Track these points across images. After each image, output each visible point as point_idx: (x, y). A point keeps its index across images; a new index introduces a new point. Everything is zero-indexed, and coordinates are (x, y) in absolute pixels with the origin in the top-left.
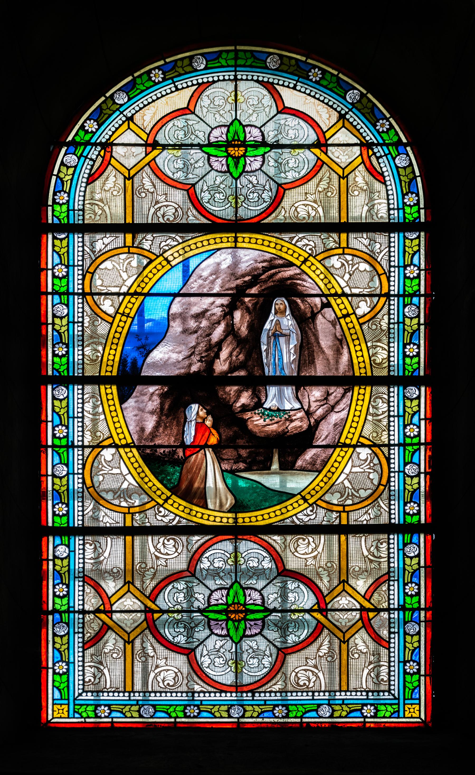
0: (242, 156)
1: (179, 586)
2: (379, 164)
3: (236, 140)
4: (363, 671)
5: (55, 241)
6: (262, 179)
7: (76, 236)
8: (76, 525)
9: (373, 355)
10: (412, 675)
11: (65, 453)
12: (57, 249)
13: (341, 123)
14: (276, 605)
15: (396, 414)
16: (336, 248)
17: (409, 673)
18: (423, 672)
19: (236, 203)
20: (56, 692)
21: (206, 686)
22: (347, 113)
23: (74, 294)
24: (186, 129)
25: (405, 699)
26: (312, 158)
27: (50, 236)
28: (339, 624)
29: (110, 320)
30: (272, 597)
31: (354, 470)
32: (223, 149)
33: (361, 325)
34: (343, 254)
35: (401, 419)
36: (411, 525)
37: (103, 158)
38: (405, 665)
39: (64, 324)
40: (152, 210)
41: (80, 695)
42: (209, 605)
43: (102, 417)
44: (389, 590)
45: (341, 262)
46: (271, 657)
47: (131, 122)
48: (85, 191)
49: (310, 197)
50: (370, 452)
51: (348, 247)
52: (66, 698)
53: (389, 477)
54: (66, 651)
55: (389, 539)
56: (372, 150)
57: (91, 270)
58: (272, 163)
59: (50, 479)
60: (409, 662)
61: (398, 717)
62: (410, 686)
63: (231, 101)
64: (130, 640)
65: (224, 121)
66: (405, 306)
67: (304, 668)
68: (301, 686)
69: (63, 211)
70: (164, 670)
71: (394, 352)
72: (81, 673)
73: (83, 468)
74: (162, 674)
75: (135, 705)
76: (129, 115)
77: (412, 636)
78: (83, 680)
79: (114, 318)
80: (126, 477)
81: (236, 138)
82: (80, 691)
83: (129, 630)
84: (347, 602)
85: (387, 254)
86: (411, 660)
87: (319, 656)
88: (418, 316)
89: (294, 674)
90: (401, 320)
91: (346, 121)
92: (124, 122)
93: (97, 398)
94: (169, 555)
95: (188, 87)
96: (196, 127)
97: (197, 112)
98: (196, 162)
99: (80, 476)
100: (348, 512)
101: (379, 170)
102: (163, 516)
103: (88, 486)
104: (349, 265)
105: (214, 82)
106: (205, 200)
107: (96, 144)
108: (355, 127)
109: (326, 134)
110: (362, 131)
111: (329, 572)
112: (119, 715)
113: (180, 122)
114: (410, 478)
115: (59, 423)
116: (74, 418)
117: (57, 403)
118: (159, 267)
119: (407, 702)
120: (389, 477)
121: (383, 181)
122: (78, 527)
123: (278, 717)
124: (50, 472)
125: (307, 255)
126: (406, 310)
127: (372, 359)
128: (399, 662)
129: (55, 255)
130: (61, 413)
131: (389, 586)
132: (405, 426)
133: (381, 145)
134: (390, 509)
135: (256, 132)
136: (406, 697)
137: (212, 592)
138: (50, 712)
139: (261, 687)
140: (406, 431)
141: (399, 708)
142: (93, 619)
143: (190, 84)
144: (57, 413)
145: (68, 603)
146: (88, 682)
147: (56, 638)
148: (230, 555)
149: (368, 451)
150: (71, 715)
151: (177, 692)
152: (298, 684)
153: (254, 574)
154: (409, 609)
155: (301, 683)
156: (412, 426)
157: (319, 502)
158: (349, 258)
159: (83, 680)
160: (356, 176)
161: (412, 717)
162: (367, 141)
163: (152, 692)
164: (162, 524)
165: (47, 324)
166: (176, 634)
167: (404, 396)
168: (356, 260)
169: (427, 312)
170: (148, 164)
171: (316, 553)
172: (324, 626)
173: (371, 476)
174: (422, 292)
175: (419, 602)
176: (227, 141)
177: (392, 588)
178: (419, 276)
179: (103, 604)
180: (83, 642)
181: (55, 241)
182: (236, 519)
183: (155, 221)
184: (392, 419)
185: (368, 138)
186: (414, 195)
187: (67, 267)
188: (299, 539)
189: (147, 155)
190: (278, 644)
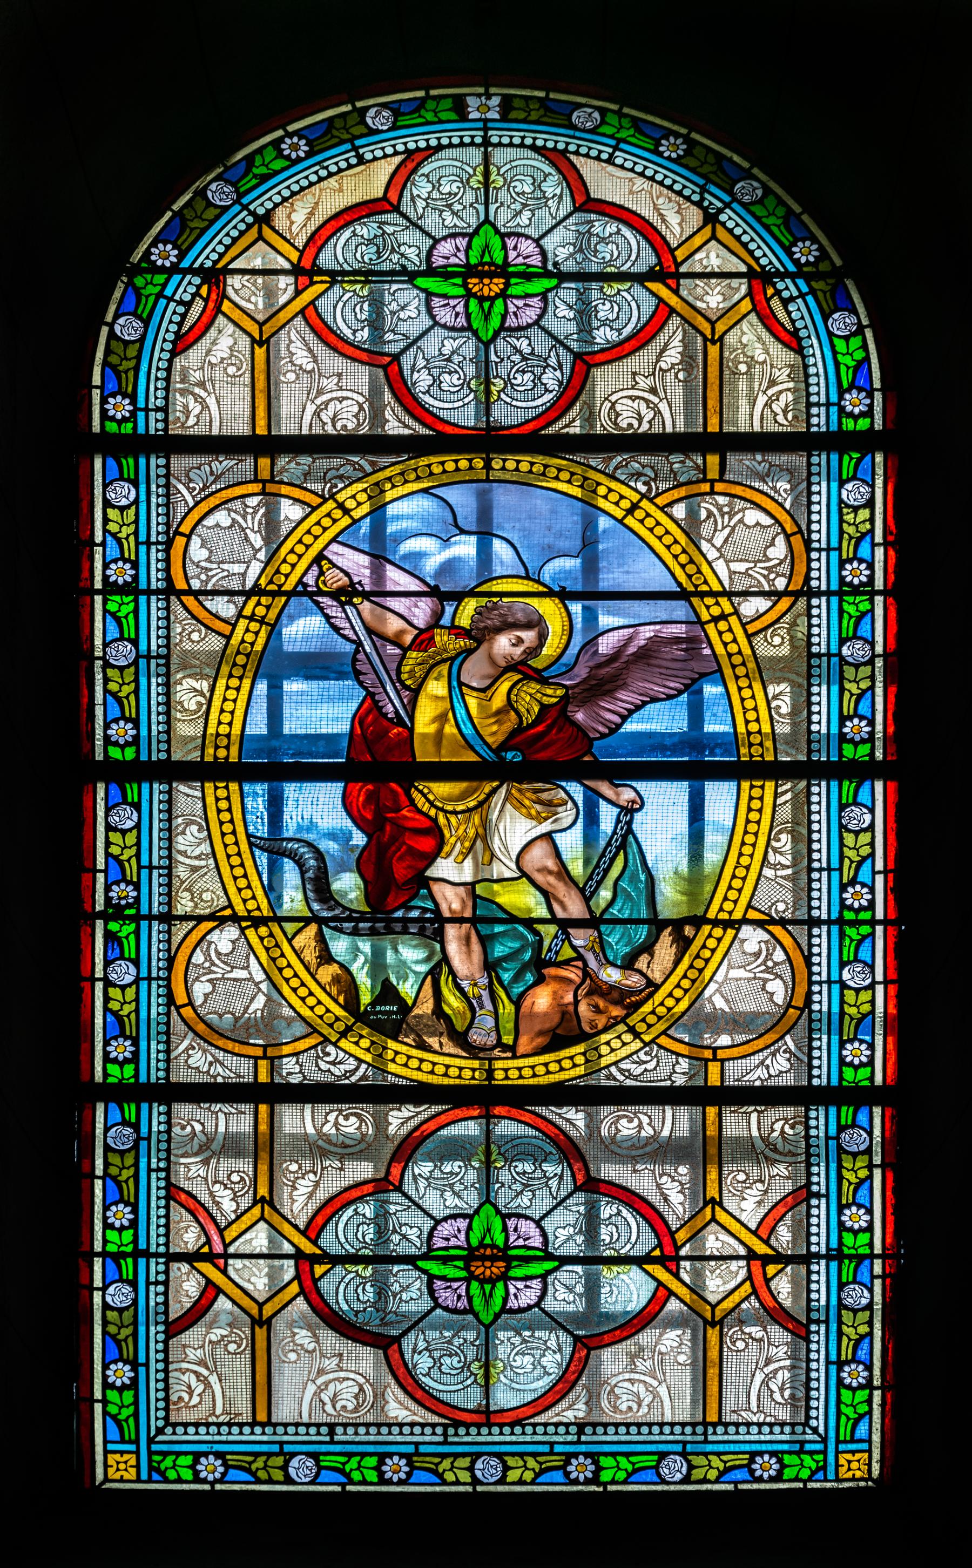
0: (497, 296)
1: (365, 231)
2: (789, 313)
3: (487, 1246)
5: (109, 511)
6: (541, 344)
9: (775, 697)
13: (708, 231)
14: (571, 1250)
16: (698, 481)
18: (877, 1383)
19: (487, 174)
21: (423, 1412)
22: (720, 211)
23: (149, 592)
24: (380, 241)
25: (838, 1442)
26: (648, 306)
28: (704, 306)
29: (227, 629)
30: (562, 1234)
31: (734, 973)
32: (458, 281)
33: (749, 637)
35: (835, 875)
36: (853, 761)
37: (206, 300)
38: (840, 1370)
40: (311, 409)
41: (160, 1431)
42: (430, 1249)
44: (809, 1216)
47: (265, 227)
50: (766, 937)
53: (809, 993)
54: (132, 697)
55: (807, 1118)
56: (774, 285)
57: (185, 529)
59: (99, 986)
60: (848, 1363)
61: (826, 1480)
63: (475, 185)
65: (460, 224)
67: (631, 393)
69: (126, 1323)
71: (818, 1380)
72: (161, 1385)
73: (170, 968)
74: (331, 406)
76: (261, 211)
77: (857, 833)
79: (234, 626)
82: (161, 1423)
84: (719, 1245)
86: (855, 557)
89: (607, 405)
91: (718, 227)
92: (249, 226)
95: (386, 156)
96: (404, 1217)
97: (403, 208)
100: (722, 1061)
101: (789, 326)
102: (333, 1063)
103: (179, 1002)
105: (440, 148)
107: (191, 270)
108: (738, 238)
110: (752, 246)
113: (366, 230)
114: (852, 835)
117: (113, 514)
118: (326, 522)
119: (842, 1447)
121: (794, 345)
124: (99, 973)
125: (635, 497)
127: (773, 705)
128: (828, 1362)
130: (123, 535)
131: (809, 1207)
133: (793, 276)
134: (811, 1058)
135: (527, 247)
137: (436, 241)
141: (825, 1460)
143: (389, 151)
145: (135, 1241)
147: (111, 990)
149: (761, 935)
150: (144, 1476)
153: (526, 1186)
154: (850, 1257)
157: (663, 1040)
160: (743, 333)
162: (763, 267)
164: (330, 1079)
165: (93, 980)
168: (739, 504)
169: (888, 1240)
170: (302, 312)
172: (672, 311)
173: (770, 987)
175: (871, 1245)
176: (469, 1247)
177: (814, 1211)
183: (317, 430)
185: (764, 261)
186: (863, 394)
188: (620, 1117)
189: (298, 293)
190: (574, 346)
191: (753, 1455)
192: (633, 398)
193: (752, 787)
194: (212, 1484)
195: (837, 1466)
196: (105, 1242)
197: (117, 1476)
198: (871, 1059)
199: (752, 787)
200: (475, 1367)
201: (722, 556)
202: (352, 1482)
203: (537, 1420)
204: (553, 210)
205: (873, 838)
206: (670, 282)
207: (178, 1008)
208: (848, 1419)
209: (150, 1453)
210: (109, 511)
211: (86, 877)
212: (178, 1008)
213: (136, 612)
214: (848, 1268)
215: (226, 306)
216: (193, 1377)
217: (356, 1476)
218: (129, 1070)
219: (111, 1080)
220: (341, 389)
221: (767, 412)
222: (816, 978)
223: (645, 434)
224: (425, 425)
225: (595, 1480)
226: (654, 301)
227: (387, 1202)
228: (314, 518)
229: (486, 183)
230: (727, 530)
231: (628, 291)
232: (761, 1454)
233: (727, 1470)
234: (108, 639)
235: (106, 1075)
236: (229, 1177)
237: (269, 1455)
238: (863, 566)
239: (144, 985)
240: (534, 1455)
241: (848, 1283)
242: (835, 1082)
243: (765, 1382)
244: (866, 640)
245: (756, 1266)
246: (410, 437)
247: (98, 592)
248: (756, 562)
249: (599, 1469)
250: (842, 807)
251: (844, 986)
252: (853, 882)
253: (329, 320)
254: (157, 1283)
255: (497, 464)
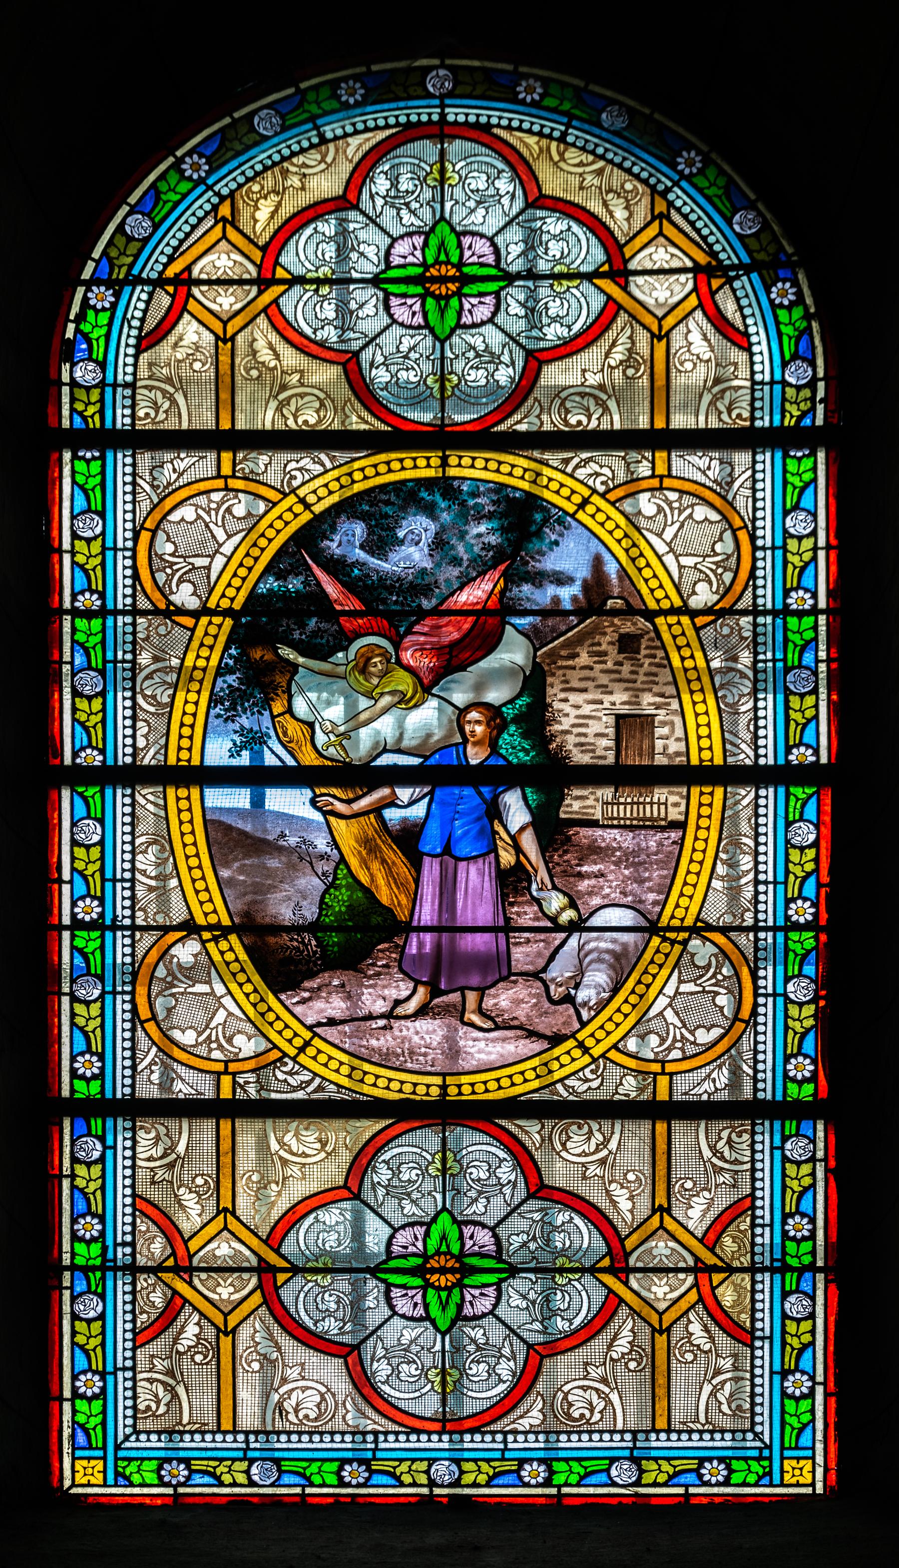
4: (701, 396)
7: (119, 792)
8: (119, 1095)
10: (797, 1400)
11: (98, 797)
12: (80, 479)
15: (771, 879)
17: (792, 1397)
20: (78, 1036)
21: (383, 1421)
25: (783, 1448)
26: (599, 1296)
27: (67, 456)
34: (661, 488)
35: (781, 888)
36: (797, 1102)
39: (93, 400)
41: (127, 1438)
42: (389, 266)
43: (174, 882)
45: (659, 506)
46: (515, 1360)
48: (135, 365)
49: (594, 1372)
51: (670, 476)
52: (100, 1445)
53: (756, 1005)
54: (99, 1350)
58: (515, 309)
59: (66, 390)
61: (771, 1485)
62: (795, 1184)
64: (228, 336)
65: (418, 223)
66: (785, 1295)
67: (581, 1383)
68: (575, 1420)
69: (93, 553)
70: (296, 395)
71: (762, 1395)
74: (294, 1396)
75: (240, 1460)
78: (135, 1407)
80: (222, 1000)
81: (443, 257)
82: (128, 1431)
83: (223, 243)
85: (748, 484)
86: (798, 1212)
87: (612, 1359)
88: (814, 533)
90: (779, 542)
93: (163, 846)
94: (307, 1156)
97: (362, 206)
98: (361, 306)
99: (127, 998)
103: (143, 1018)
104: (672, 509)
106: (381, 1376)
109: (625, 250)
111: (627, 201)
112: (207, 1480)
115: (86, 1366)
116: (114, 880)
117: (80, 1326)
118: (288, 516)
119: (787, 1453)
120: (756, 1005)
122: (122, 431)
123: (527, 1485)
126: (790, 677)
129: (78, 1034)
130: (89, 486)
132: (788, 901)
136: (787, 1445)
138: (67, 1473)
139: (494, 1421)
140: (789, 1067)
141: (771, 1466)
142: (154, 1285)
144: (81, 1029)
146: (145, 1412)
148: (431, 166)
151: (321, 1433)
152: (569, 1416)
155: (576, 1415)
156: (800, 1059)
157: (613, 1054)
158: (673, 496)
159: (135, 1407)
160: (690, 1322)
161: (798, 1485)
163: (274, 1432)
165: (61, 1176)
166: (321, 1316)
167: (787, 842)
168: (687, 500)
170: (265, 310)
171: (604, 1153)
172: (620, 307)
174: (820, 1263)
178: (811, 1394)
179: (174, 1254)
180: (133, 1330)
181: (76, 849)
182: (444, 464)
184: (762, 888)
187: (103, 1375)
191: (702, 1461)
192: (584, 1388)
193: (702, 794)
194: (175, 1487)
195: (782, 1472)
196: (73, 1255)
197: (84, 1481)
198: (813, 1232)
199: (702, 794)
200: (432, 1373)
201: (671, 550)
202: (312, 1485)
203: (493, 1427)
204: (506, 208)
205: (814, 1326)
206: (623, 1276)
207: (142, 1023)
208: (795, 488)
209: (116, 1459)
210: (77, 1323)
211: (55, 1405)
212: (142, 1023)
213: (102, 947)
214: (791, 1280)
215: (192, 305)
216: (159, 395)
217: (317, 1480)
218: (95, 1086)
219: (77, 1096)
220: (303, 1378)
221: (713, 1404)
222: (760, 543)
223: (594, 431)
224: (383, 421)
225: (548, 1483)
226: (602, 298)
227: (346, 220)
228: (276, 512)
229: (442, 180)
230: (677, 525)
231: (577, 287)
232: (710, 1460)
233: (677, 1474)
234: (76, 512)
235: (73, 1091)
236: (193, 1181)
237: (234, 1460)
238: (805, 1220)
239: (109, 998)
240: (488, 1461)
241: (795, 821)
242: (779, 1097)
243: (713, 1394)
244: (809, 512)
245: (702, 277)
246: (370, 431)
247: (66, 928)
248: (705, 557)
249: (551, 1472)
250: (788, 824)
251: (787, 1000)
252: (796, 507)
253: (291, 318)
254: (124, 1369)
255: (453, 461)
